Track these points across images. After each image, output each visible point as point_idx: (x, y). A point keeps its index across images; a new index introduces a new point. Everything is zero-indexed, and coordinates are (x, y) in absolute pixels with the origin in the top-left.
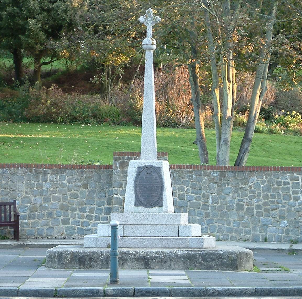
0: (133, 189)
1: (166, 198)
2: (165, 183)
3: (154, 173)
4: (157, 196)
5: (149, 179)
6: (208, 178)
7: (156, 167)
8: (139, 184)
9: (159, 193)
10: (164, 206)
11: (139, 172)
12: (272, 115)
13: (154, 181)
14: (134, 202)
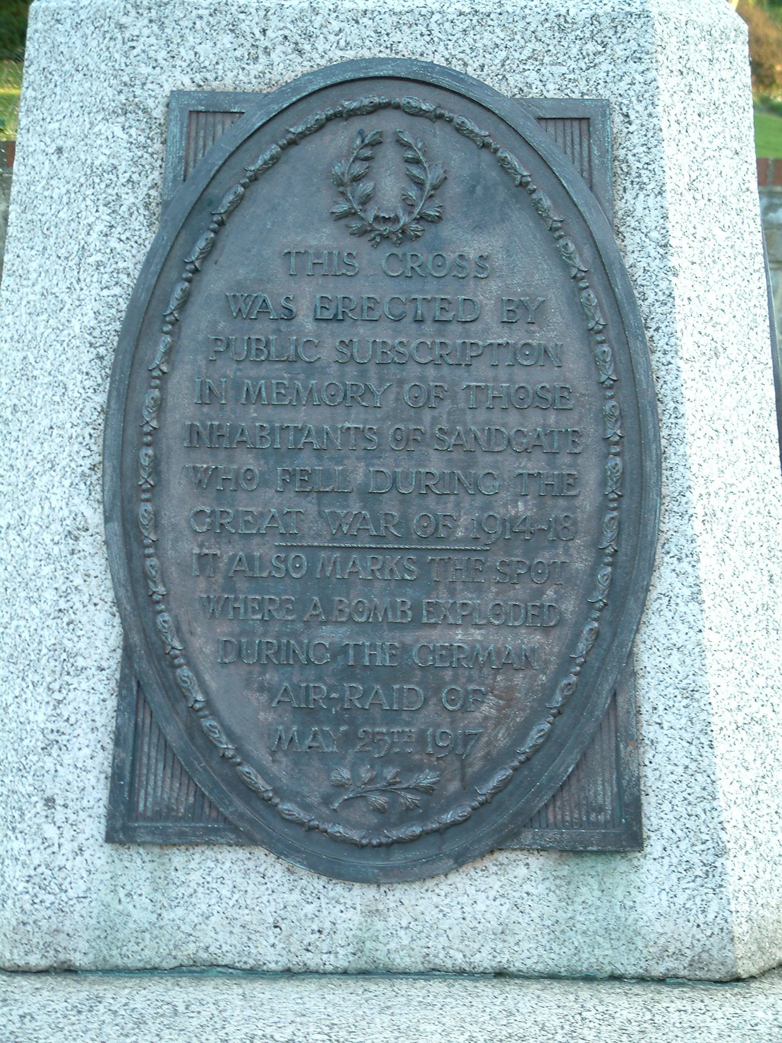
0: (94, 517)
1: (690, 693)
2: (686, 409)
3: (479, 227)
4: (526, 660)
5: (384, 333)
6: (568, 616)
7: (524, 103)
8: (194, 436)
9: (569, 606)
10: (654, 846)
11: (203, 202)
12: (595, 699)
13: (482, 371)
14: (103, 761)
